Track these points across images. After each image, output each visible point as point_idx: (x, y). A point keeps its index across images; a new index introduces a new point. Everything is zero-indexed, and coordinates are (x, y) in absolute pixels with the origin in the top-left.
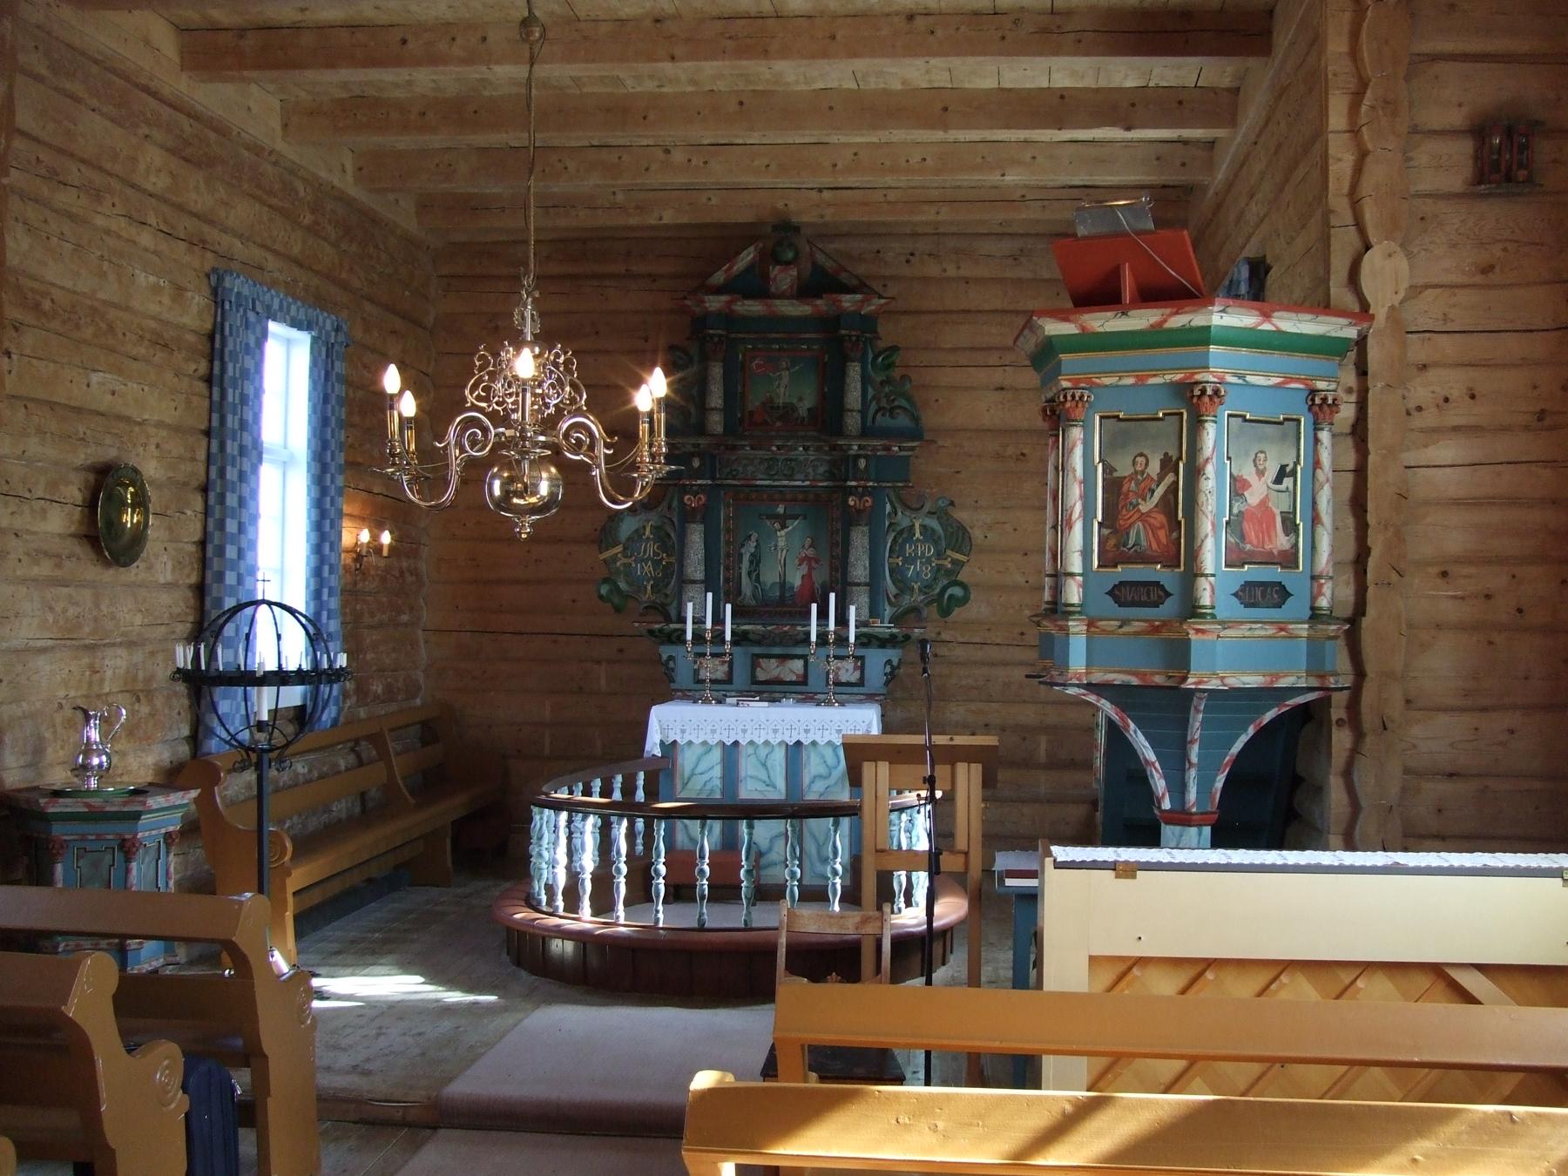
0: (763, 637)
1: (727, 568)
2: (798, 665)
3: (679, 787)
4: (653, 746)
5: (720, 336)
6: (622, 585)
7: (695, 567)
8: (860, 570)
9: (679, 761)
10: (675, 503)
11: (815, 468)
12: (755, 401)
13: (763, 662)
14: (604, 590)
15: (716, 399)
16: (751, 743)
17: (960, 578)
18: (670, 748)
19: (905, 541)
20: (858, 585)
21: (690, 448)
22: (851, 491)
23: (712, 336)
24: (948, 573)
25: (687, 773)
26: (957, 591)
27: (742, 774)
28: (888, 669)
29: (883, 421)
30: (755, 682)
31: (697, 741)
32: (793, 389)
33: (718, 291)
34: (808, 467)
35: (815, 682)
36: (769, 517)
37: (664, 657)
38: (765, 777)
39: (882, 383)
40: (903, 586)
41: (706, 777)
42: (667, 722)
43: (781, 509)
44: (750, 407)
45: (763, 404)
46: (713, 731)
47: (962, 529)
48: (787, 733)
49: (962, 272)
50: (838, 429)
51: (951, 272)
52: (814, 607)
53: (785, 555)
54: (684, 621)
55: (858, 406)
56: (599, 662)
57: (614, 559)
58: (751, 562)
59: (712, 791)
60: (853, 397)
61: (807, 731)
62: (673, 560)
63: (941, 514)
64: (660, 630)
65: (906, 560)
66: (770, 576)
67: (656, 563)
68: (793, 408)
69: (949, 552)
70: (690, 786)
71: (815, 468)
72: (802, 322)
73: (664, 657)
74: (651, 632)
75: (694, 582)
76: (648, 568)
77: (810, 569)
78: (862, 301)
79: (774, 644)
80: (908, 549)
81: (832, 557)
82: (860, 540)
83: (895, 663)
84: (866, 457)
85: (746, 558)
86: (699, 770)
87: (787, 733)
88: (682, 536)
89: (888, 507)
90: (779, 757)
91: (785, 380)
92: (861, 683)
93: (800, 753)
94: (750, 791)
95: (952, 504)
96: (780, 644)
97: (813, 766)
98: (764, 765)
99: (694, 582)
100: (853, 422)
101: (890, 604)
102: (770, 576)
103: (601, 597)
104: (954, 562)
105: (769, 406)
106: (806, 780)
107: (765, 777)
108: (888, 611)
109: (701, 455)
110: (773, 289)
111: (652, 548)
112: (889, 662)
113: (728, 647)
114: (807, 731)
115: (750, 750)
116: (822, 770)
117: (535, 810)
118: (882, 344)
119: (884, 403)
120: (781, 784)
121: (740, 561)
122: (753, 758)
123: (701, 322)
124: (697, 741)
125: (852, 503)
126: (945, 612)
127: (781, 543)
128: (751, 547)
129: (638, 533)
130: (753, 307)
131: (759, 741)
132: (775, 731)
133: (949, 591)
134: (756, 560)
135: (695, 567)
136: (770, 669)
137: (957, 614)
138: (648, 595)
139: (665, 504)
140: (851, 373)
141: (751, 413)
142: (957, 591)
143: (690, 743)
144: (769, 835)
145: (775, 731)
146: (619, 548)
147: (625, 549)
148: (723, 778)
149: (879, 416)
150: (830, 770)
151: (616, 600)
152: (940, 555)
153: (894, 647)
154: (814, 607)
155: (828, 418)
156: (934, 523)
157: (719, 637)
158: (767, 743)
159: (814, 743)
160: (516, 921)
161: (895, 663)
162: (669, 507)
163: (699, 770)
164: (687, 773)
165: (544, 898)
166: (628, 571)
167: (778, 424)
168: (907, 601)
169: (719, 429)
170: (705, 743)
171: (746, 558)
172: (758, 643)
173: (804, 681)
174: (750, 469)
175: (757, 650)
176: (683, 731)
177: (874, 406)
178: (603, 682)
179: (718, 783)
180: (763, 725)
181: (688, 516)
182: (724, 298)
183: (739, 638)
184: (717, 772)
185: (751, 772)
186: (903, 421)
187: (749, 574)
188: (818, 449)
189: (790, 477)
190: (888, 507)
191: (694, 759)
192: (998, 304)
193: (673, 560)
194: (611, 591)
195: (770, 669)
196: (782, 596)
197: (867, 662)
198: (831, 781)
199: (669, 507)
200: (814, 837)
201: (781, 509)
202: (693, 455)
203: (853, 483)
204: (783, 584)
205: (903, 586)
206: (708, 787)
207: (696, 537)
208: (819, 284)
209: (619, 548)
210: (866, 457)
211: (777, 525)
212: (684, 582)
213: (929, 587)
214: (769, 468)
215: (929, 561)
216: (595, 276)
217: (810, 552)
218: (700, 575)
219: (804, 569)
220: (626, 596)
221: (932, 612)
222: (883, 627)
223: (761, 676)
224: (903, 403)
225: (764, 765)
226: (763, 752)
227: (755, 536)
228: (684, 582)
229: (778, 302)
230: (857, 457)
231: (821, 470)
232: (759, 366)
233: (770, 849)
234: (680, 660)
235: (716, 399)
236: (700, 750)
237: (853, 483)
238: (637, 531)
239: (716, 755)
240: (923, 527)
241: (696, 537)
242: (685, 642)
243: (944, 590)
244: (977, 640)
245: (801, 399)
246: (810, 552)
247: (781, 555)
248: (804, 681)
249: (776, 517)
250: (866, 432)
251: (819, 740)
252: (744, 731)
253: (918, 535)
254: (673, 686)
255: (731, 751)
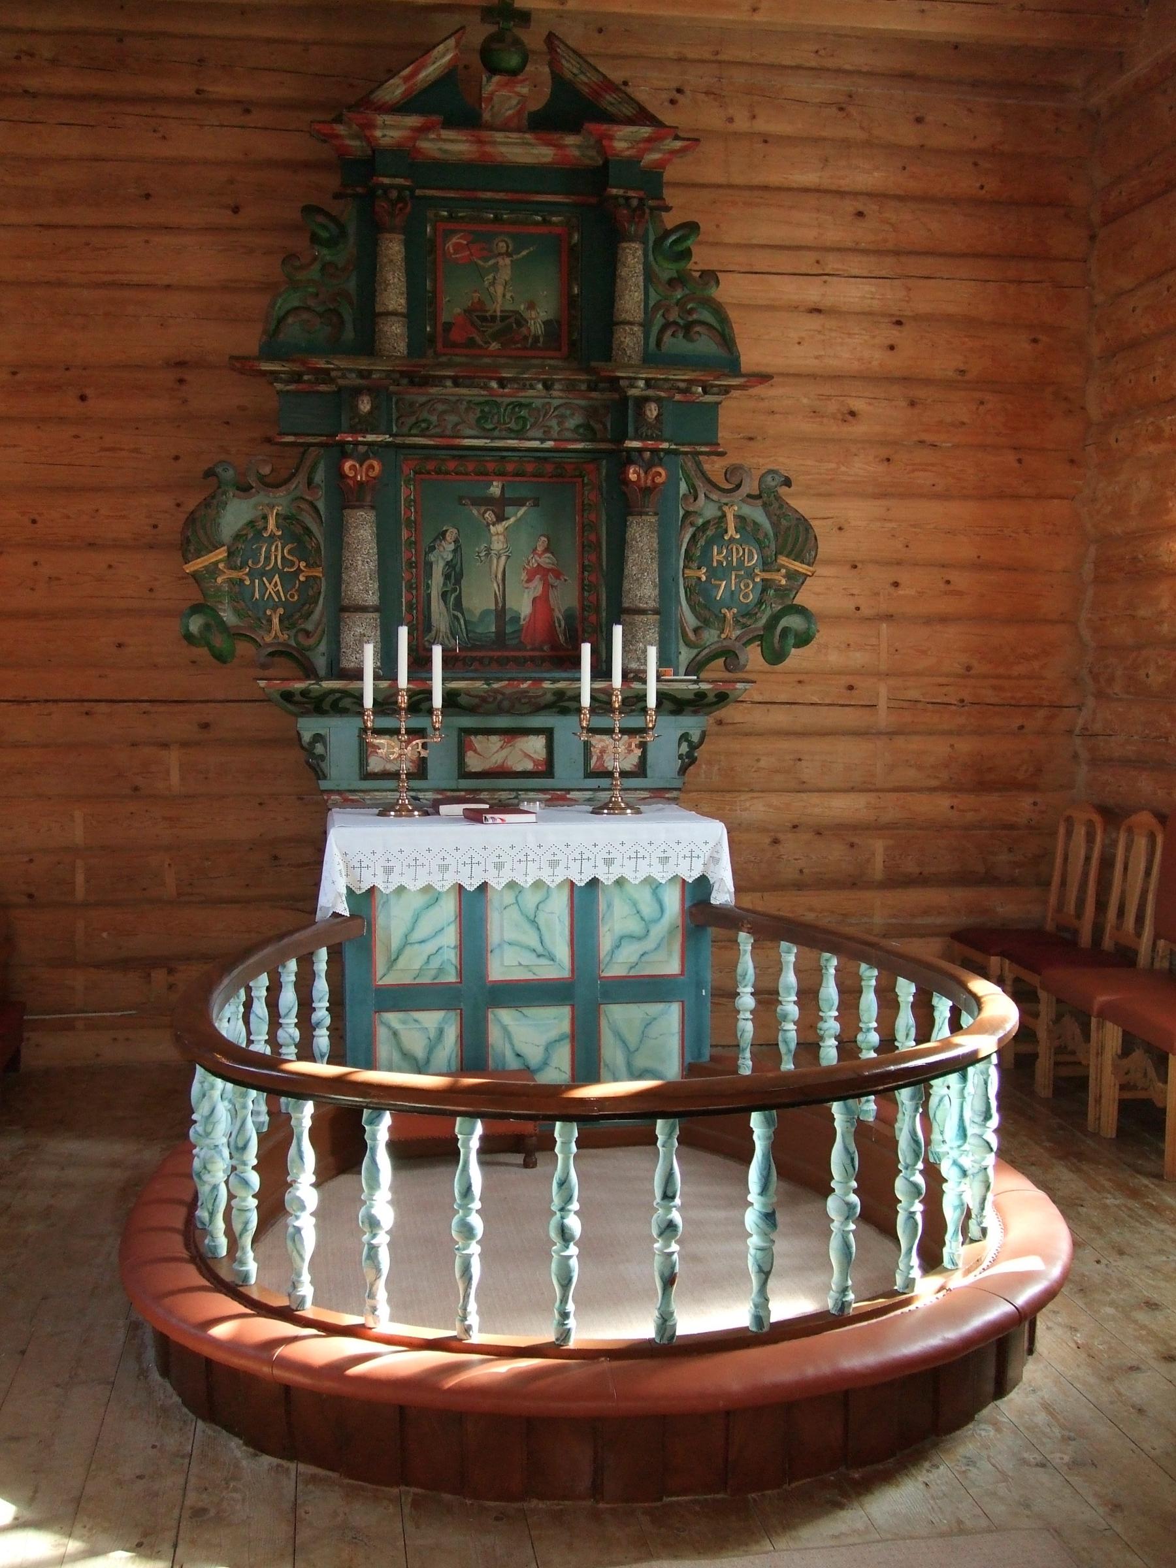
0: (484, 700)
1: (410, 588)
2: (536, 745)
3: (380, 968)
4: (333, 897)
5: (400, 188)
6: (228, 616)
7: (362, 580)
8: (643, 588)
9: (380, 921)
10: (319, 477)
11: (561, 419)
12: (452, 308)
13: (478, 741)
14: (195, 625)
15: (394, 297)
16: (512, 885)
17: (799, 600)
18: (364, 901)
19: (710, 543)
20: (643, 612)
21: (353, 380)
22: (630, 458)
23: (386, 189)
24: (782, 592)
25: (395, 944)
26: (794, 622)
27: (494, 937)
28: (685, 748)
29: (674, 343)
30: (464, 774)
31: (413, 886)
32: (518, 287)
33: (401, 108)
34: (553, 420)
35: (567, 770)
36: (477, 502)
37: (307, 737)
38: (534, 942)
39: (671, 283)
40: (708, 613)
41: (430, 947)
42: (361, 853)
43: (495, 489)
44: (445, 317)
45: (468, 311)
46: (444, 868)
47: (803, 524)
48: (575, 866)
49: (761, 125)
50: (606, 350)
51: (742, 124)
52: (586, 649)
53: (508, 567)
54: (358, 675)
55: (639, 316)
56: (165, 745)
57: (213, 570)
58: (447, 577)
59: (441, 970)
60: (632, 299)
61: (609, 862)
62: (318, 572)
63: (766, 497)
64: (304, 693)
65: (713, 573)
66: (479, 600)
67: (288, 579)
68: (521, 321)
69: (782, 560)
70: (401, 963)
71: (561, 419)
72: (536, 174)
73: (307, 737)
74: (287, 696)
75: (364, 609)
76: (274, 587)
77: (547, 586)
78: (649, 140)
79: (500, 711)
80: (717, 555)
81: (584, 568)
82: (643, 537)
83: (695, 739)
84: (658, 400)
85: (438, 570)
86: (417, 936)
87: (575, 866)
88: (338, 534)
89: (683, 487)
90: (559, 905)
91: (505, 274)
92: (641, 770)
93: (594, 902)
94: (504, 966)
95: (787, 482)
96: (510, 712)
97: (616, 921)
98: (533, 922)
99: (364, 609)
100: (630, 341)
101: (689, 644)
102: (479, 600)
103: (189, 637)
104: (792, 575)
105: (478, 315)
106: (606, 943)
107: (534, 942)
108: (685, 655)
109: (373, 391)
110: (486, 116)
111: (278, 553)
112: (685, 737)
113: (437, 719)
114: (609, 862)
115: (509, 898)
116: (633, 926)
117: (199, 1070)
118: (670, 220)
119: (674, 316)
120: (562, 952)
121: (430, 576)
122: (514, 913)
123: (361, 171)
124: (413, 886)
125: (633, 477)
126: (776, 656)
127: (498, 545)
128: (446, 549)
129: (255, 529)
130: (454, 145)
131: (526, 882)
132: (554, 864)
133: (784, 622)
134: (454, 574)
135: (362, 580)
136: (489, 752)
137: (797, 657)
138: (275, 633)
139: (301, 478)
140: (631, 260)
141: (448, 327)
142: (794, 622)
143: (401, 889)
144: (543, 1039)
145: (554, 864)
146: (221, 554)
147: (230, 554)
148: (461, 947)
149: (667, 337)
150: (648, 924)
151: (219, 641)
152: (767, 565)
153: (695, 713)
154: (586, 649)
155: (585, 333)
156: (757, 514)
157: (420, 702)
158: (538, 884)
159: (620, 882)
160: (215, 1342)
161: (695, 739)
162: (310, 483)
163: (417, 936)
164: (395, 944)
165: (222, 1242)
166: (237, 590)
167: (494, 346)
168: (710, 636)
169: (402, 347)
170: (428, 889)
171: (438, 570)
172: (471, 710)
173: (547, 769)
174: (452, 419)
175: (467, 722)
176: (388, 870)
177: (659, 321)
178: (175, 777)
179: (451, 956)
180: (534, 851)
181: (347, 496)
182: (413, 121)
183: (450, 698)
184: (450, 937)
185: (510, 935)
186: (705, 345)
187: (444, 595)
188: (571, 387)
189: (520, 434)
190: (683, 487)
191: (408, 916)
192: (810, 178)
193: (318, 572)
194: (207, 627)
195: (489, 752)
196: (500, 634)
197: (557, 736)
198: (649, 944)
199: (310, 483)
200: (618, 1035)
201: (495, 489)
202: (357, 392)
203: (636, 444)
204: (501, 612)
205: (708, 613)
206: (435, 964)
207: (363, 531)
208: (573, 107)
209: (221, 554)
210: (658, 400)
211: (490, 516)
212: (342, 609)
213: (749, 614)
214: (484, 417)
215: (751, 574)
216: (137, 99)
217: (546, 560)
218: (372, 599)
219: (537, 587)
220: (236, 635)
221: (753, 656)
222: (685, 685)
223: (474, 763)
224: (706, 316)
225: (533, 922)
226: (530, 900)
227: (452, 534)
228: (342, 609)
229: (499, 136)
230: (642, 401)
231: (571, 423)
232: (458, 247)
233: (545, 1063)
234: (334, 741)
235: (394, 297)
236: (420, 901)
237: (636, 444)
238: (251, 524)
239: (448, 907)
240: (741, 519)
241: (363, 531)
242: (579, 710)
243: (775, 619)
244: (783, 698)
245: (531, 306)
246: (546, 560)
247: (498, 565)
248: (547, 769)
249: (488, 501)
250: (649, 359)
251: (629, 875)
252: (499, 866)
253: (732, 531)
254: (324, 785)
255: (472, 904)
